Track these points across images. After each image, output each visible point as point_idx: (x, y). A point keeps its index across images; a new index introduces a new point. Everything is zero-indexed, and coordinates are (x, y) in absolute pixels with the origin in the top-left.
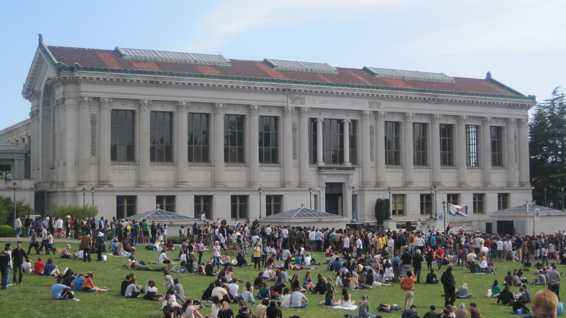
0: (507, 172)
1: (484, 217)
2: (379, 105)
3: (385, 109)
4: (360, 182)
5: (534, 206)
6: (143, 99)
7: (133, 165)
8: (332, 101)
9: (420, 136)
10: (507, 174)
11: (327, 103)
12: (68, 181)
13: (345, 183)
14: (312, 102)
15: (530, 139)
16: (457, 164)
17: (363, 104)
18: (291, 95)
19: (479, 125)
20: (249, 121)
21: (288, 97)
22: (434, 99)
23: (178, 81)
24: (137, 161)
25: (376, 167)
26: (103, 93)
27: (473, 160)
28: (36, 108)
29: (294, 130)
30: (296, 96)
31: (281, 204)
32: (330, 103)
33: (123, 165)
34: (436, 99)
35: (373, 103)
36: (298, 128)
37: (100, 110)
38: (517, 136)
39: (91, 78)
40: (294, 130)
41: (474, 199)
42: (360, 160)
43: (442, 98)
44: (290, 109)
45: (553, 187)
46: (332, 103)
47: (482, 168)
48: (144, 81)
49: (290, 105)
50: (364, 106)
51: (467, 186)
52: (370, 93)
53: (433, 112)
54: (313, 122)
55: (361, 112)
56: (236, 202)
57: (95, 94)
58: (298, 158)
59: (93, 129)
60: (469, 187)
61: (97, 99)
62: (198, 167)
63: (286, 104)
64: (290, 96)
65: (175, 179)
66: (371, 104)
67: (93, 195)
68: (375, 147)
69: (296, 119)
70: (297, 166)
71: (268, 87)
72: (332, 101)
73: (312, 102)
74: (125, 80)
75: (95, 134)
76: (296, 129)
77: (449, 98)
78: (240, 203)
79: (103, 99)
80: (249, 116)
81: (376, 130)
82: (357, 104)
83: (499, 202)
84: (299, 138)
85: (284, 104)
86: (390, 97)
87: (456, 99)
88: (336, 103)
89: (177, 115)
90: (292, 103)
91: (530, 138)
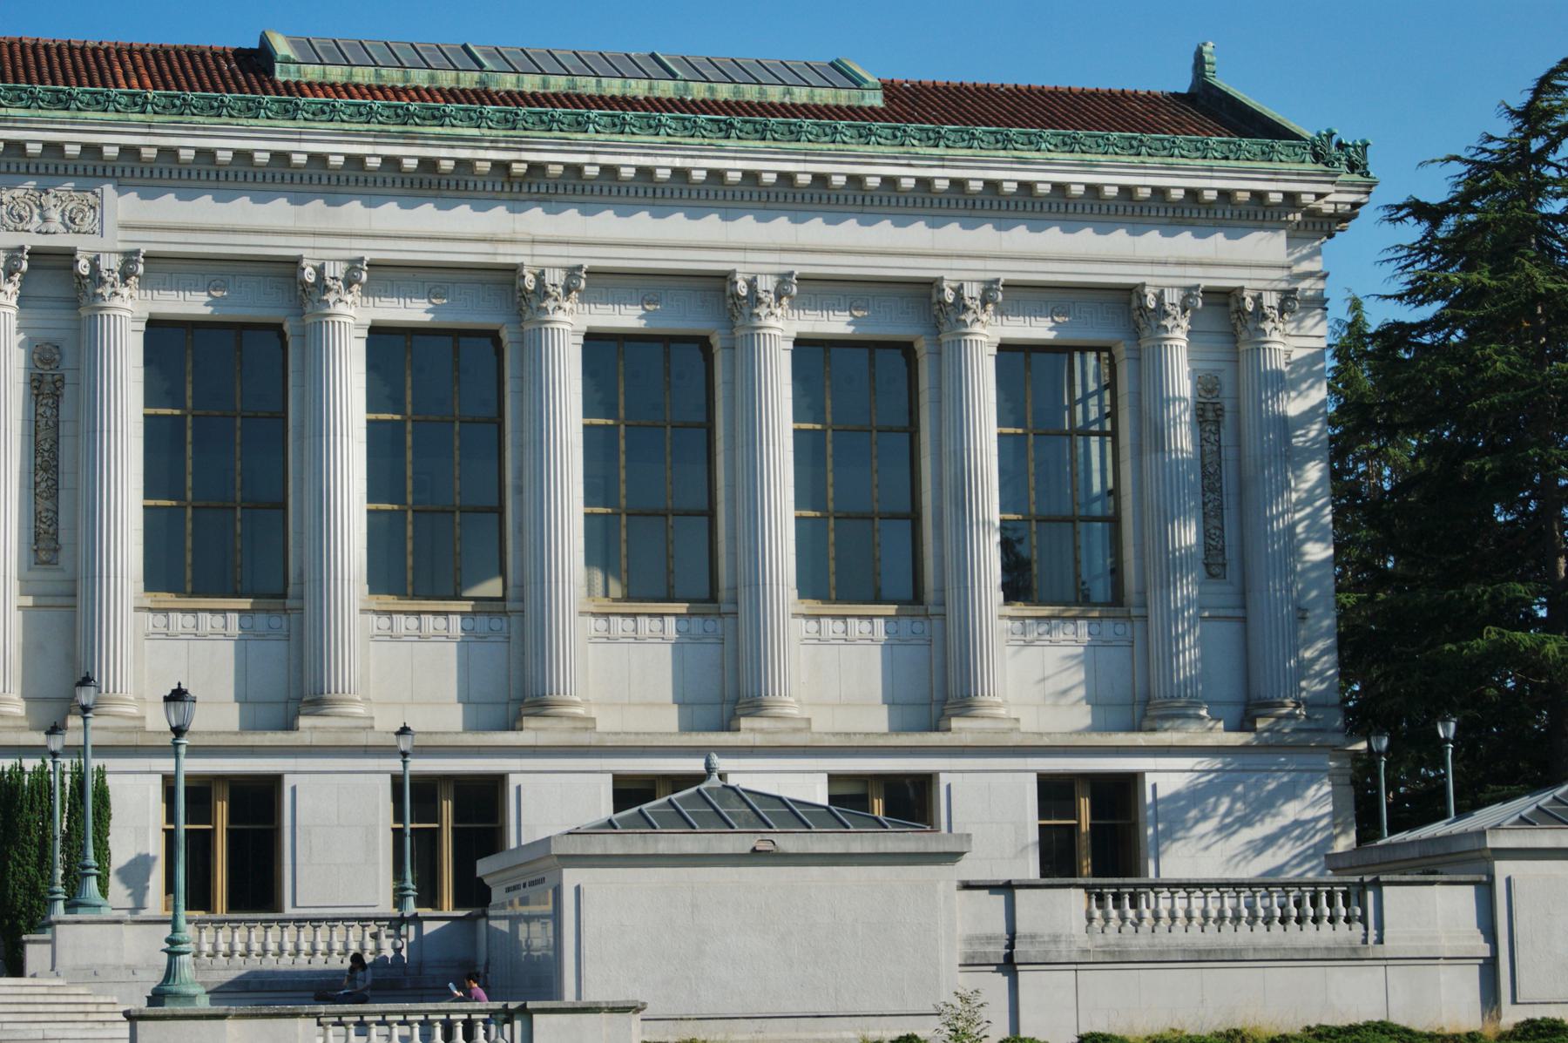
0: (1138, 634)
5: (1193, 856)
25: (1239, 613)
28: (84, 313)
29: (1210, 415)
36: (1228, 405)
40: (1210, 415)
47: (725, 608)
51: (780, 725)
56: (208, 817)
58: (1232, 570)
60: (796, 730)
70: (1230, 613)
71: (688, 163)
87: (678, 163)
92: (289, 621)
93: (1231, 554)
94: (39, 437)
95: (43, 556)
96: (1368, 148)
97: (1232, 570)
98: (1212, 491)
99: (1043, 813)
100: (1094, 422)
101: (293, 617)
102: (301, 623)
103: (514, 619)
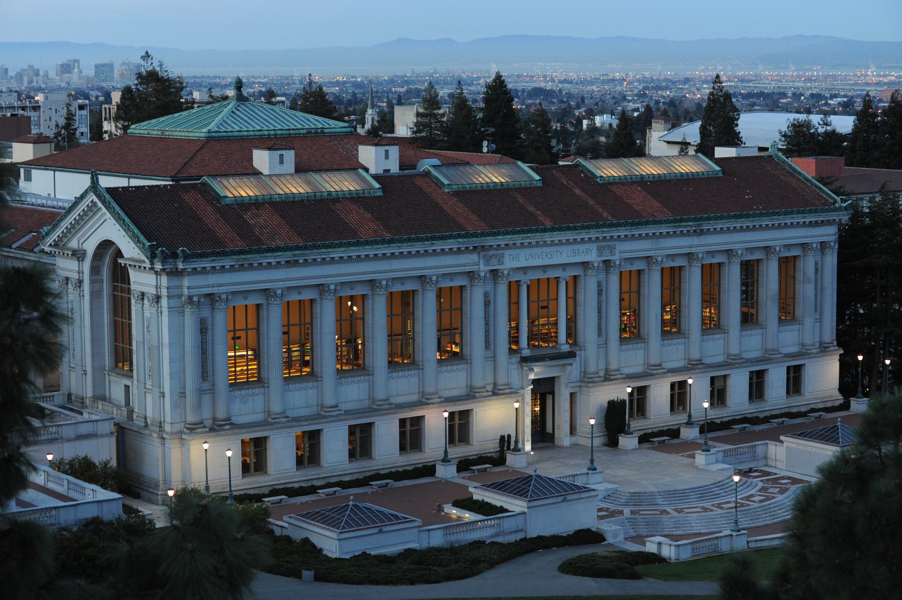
1: (761, 408)
2: (612, 249)
3: (622, 254)
4: (581, 372)
6: (275, 287)
7: (415, 370)
9: (671, 286)
10: (726, 340)
11: (537, 257)
13: (558, 377)
14: (515, 259)
16: (687, 329)
17: (589, 252)
18: (485, 253)
19: (366, 293)
21: (479, 256)
22: (695, 231)
23: (324, 256)
26: (219, 285)
29: (487, 303)
30: (491, 253)
33: (246, 389)
34: (698, 231)
35: (603, 247)
36: (492, 300)
37: (213, 310)
38: (819, 268)
39: (204, 268)
41: (751, 378)
42: (580, 338)
43: (707, 228)
44: (482, 274)
45: (881, 340)
46: (544, 257)
48: (286, 262)
49: (483, 269)
50: (591, 254)
52: (600, 235)
53: (693, 250)
54: (514, 288)
55: (585, 265)
56: (404, 427)
57: (207, 289)
59: (203, 341)
61: (210, 296)
62: (350, 379)
63: (477, 267)
64: (483, 254)
65: (318, 402)
66: (600, 250)
68: (604, 315)
69: (818, 258)
71: (452, 247)
72: (544, 254)
74: (467, 248)
75: (206, 349)
77: (718, 226)
80: (423, 291)
81: (606, 287)
82: (580, 253)
83: (672, 396)
84: (494, 315)
85: (474, 267)
86: (630, 236)
89: (321, 303)
90: (598, 256)
101: (764, 330)
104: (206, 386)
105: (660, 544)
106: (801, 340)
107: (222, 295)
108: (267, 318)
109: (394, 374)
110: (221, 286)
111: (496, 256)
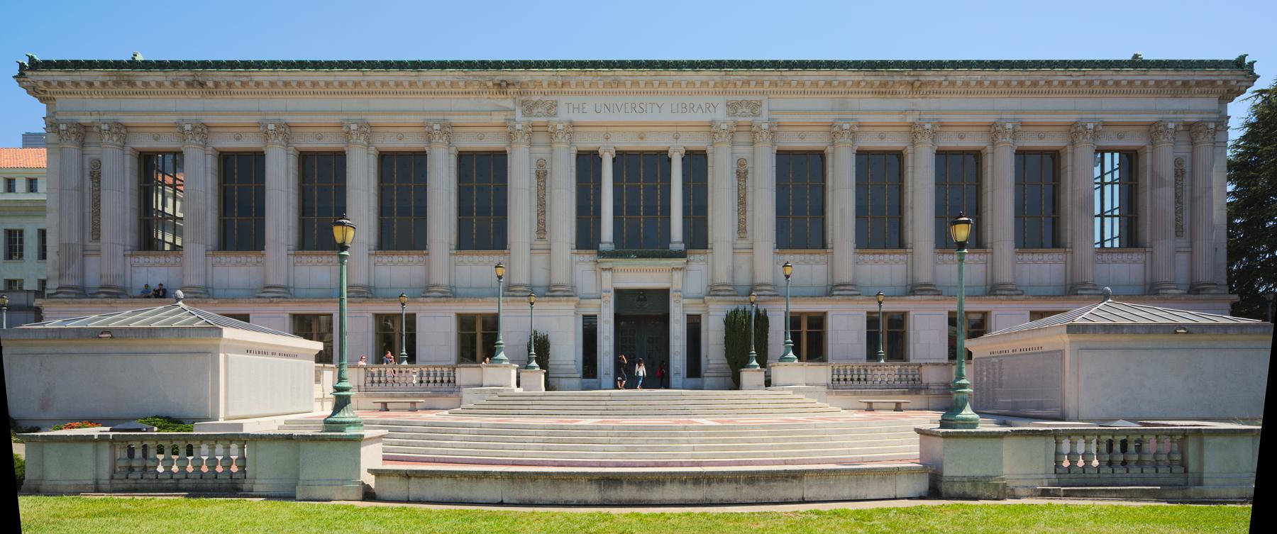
0: (989, 260)
8: (629, 106)
10: (989, 264)
11: (616, 109)
12: (168, 280)
14: (576, 111)
15: (1233, 193)
20: (833, 161)
24: (909, 246)
25: (1190, 250)
27: (97, 253)
29: (1180, 174)
31: (825, 332)
32: (623, 110)
36: (1187, 170)
40: (1180, 174)
46: (629, 110)
54: (588, 163)
58: (1187, 233)
62: (314, 259)
65: (907, 282)
67: (532, 308)
69: (1183, 150)
70: (1186, 250)
72: (629, 106)
73: (576, 111)
76: (1183, 172)
78: (808, 329)
79: (97, 127)
82: (695, 109)
88: (638, 109)
91: (1230, 188)
92: (907, 258)
93: (1186, 227)
94: (740, 192)
95: (95, 237)
96: (17, 73)
97: (1187, 233)
98: (1179, 203)
99: (867, 329)
100: (1117, 179)
101: (989, 255)
102: (833, 257)
103: (909, 255)
104: (542, 244)
105: (142, 478)
106: (909, 276)
107: (1170, 124)
108: (833, 167)
109: (1026, 257)
110: (1188, 113)
111: (544, 103)
